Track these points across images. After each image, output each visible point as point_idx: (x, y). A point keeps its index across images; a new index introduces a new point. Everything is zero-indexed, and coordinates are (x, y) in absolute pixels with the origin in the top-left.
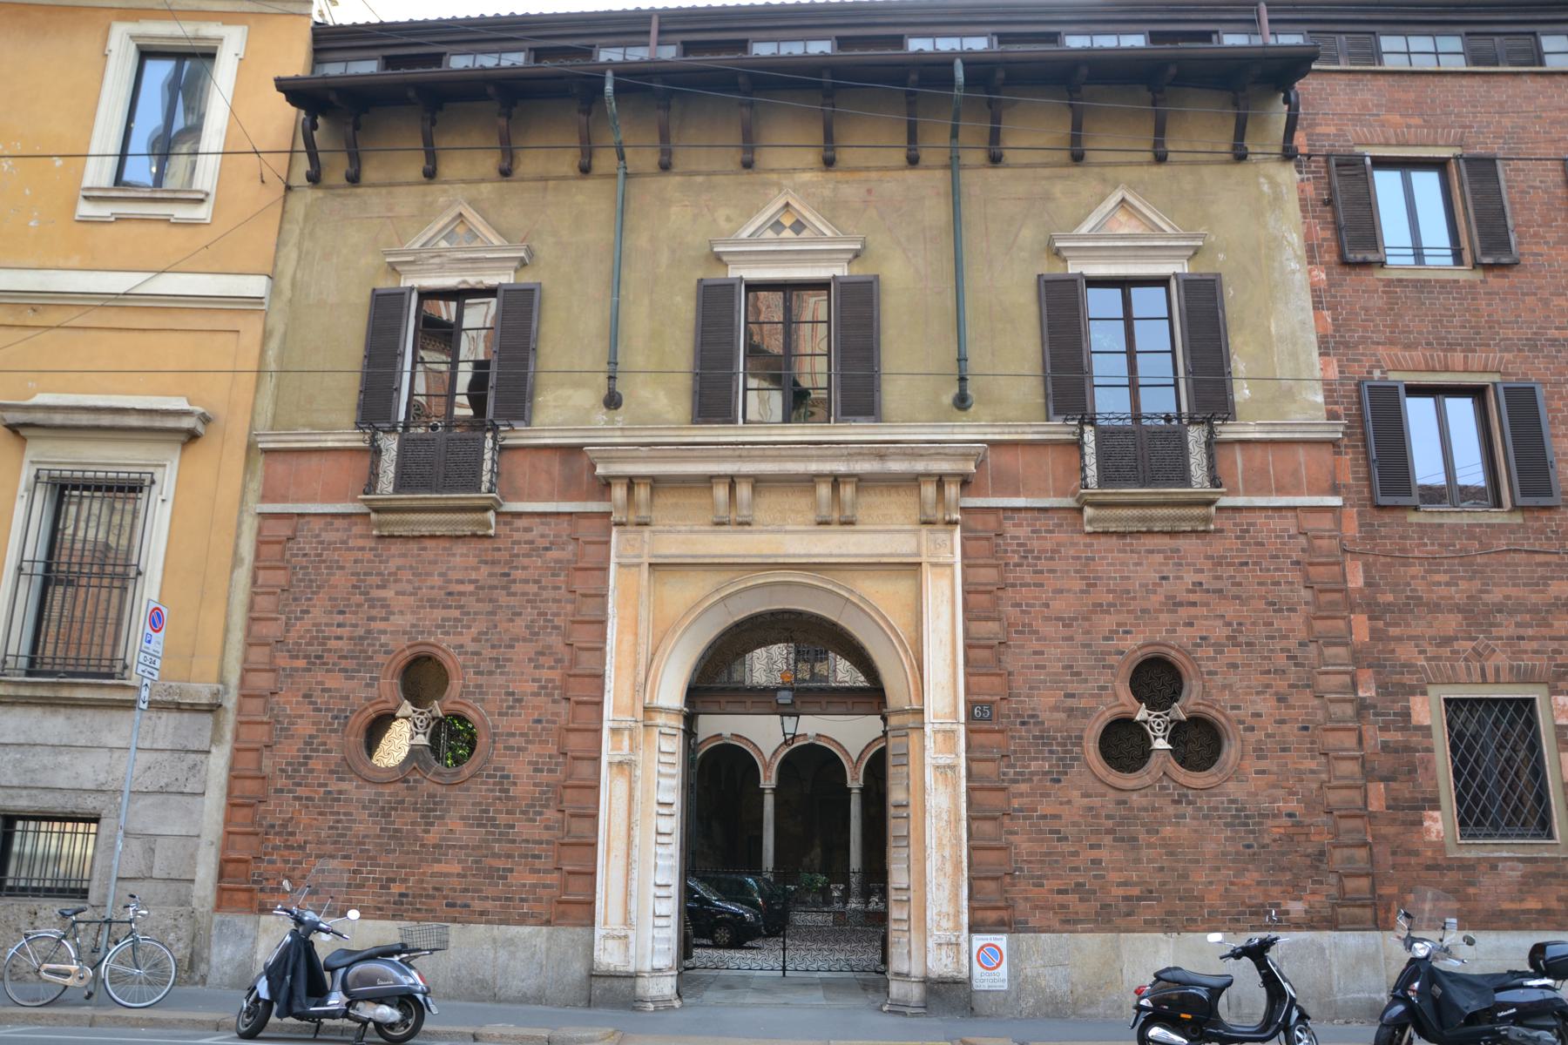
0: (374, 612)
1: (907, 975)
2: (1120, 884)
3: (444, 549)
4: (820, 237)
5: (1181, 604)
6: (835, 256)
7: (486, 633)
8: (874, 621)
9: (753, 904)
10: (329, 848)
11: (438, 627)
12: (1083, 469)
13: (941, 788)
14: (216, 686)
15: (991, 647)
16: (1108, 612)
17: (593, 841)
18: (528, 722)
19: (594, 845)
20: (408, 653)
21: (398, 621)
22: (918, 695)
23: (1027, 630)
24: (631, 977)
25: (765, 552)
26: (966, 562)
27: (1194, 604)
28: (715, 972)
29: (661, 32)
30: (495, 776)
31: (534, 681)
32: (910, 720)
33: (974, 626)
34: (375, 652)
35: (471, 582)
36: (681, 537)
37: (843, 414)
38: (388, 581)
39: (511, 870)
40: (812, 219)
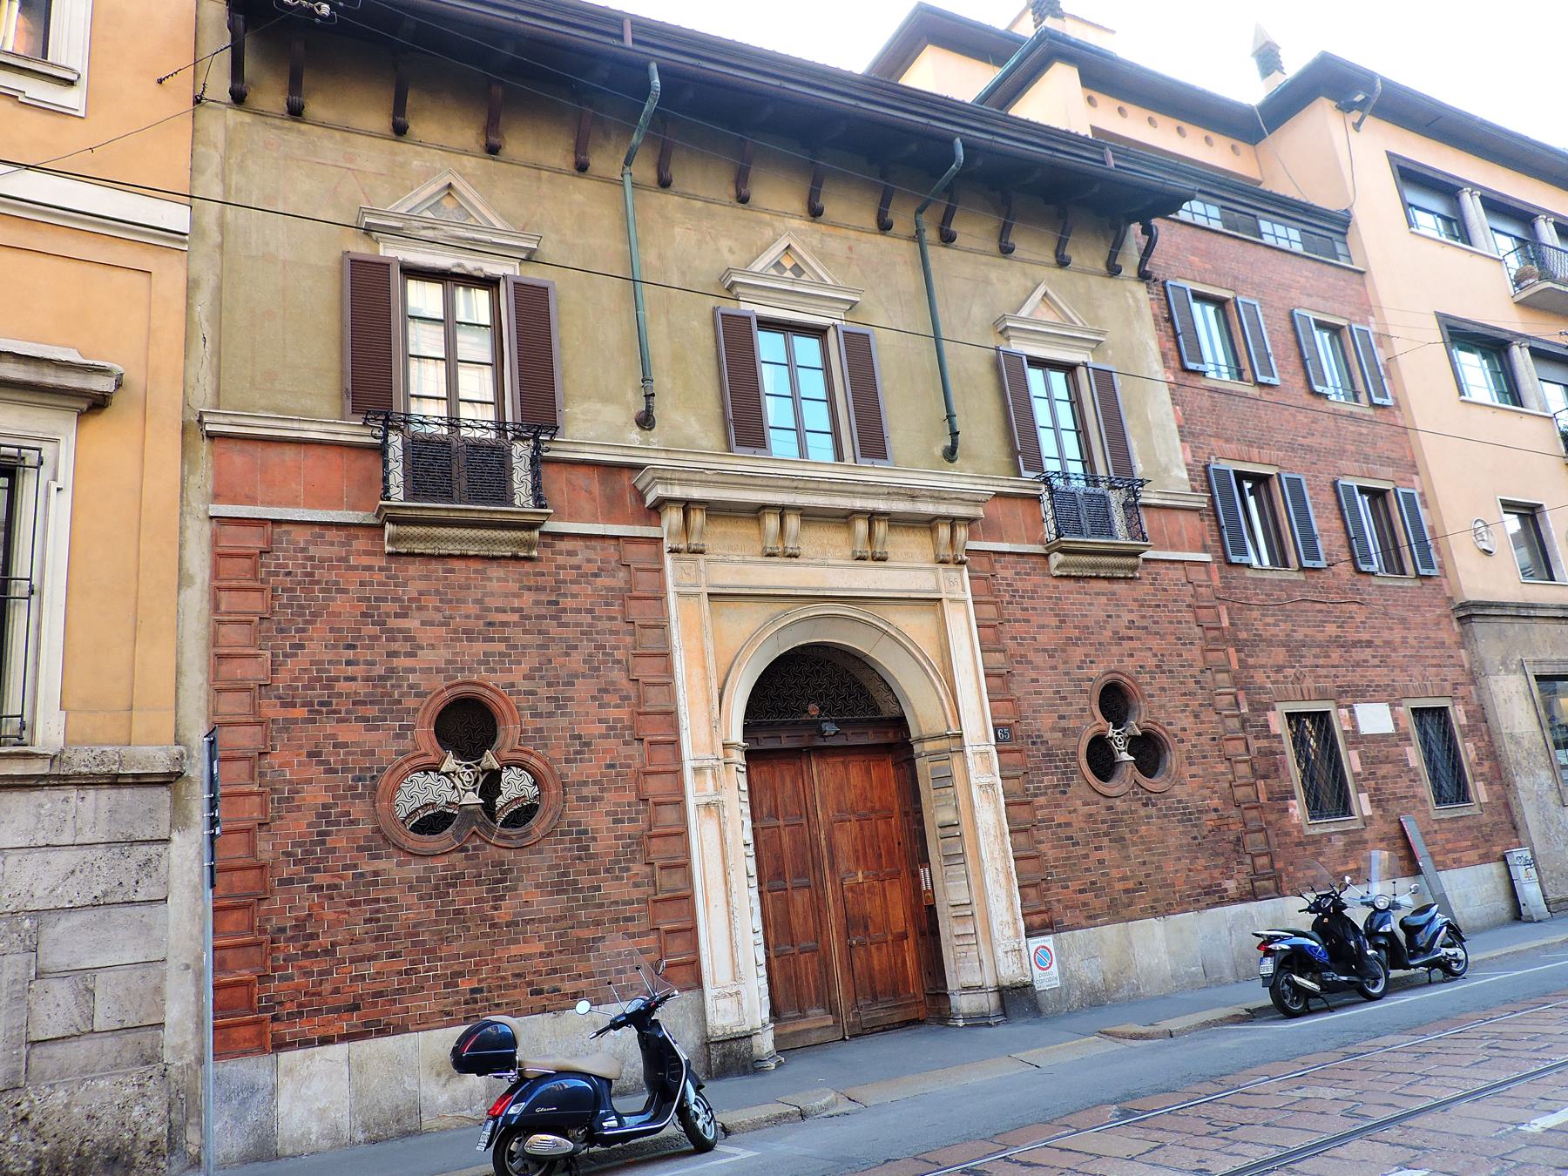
0: (395, 646)
2: (1121, 879)
3: (476, 571)
5: (1122, 638)
7: (540, 669)
10: (368, 947)
11: (480, 663)
13: (986, 805)
14: (176, 750)
17: (688, 892)
18: (600, 768)
20: (446, 694)
21: (427, 657)
23: (1023, 660)
27: (1131, 638)
31: (600, 721)
34: (402, 695)
35: (514, 610)
38: (409, 608)
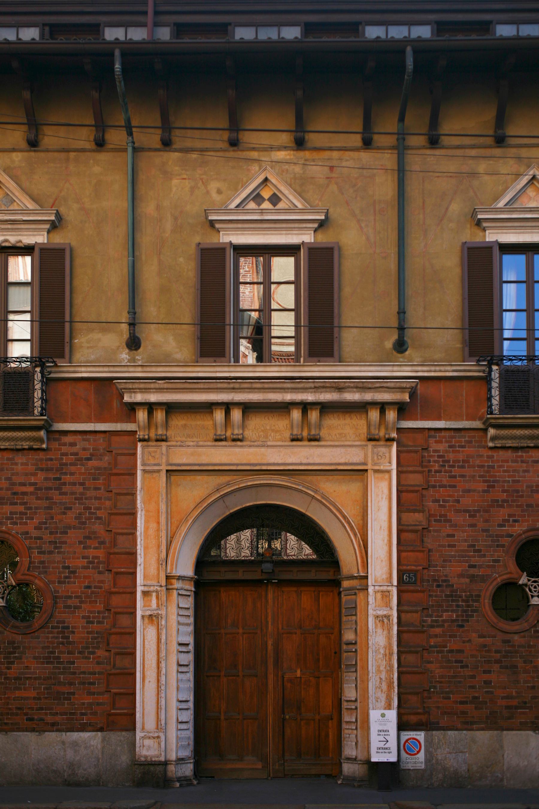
1: (355, 759)
2: (503, 698)
3: (8, 459)
4: (293, 209)
6: (304, 225)
7: (45, 523)
8: (332, 512)
11: (8, 518)
12: (489, 399)
13: (380, 631)
15: (416, 531)
16: (502, 506)
18: (81, 588)
22: (363, 566)
25: (252, 462)
29: (157, 13)
30: (58, 627)
31: (84, 558)
32: (354, 583)
35: (31, 484)
36: (190, 450)
39: (73, 694)
40: (286, 192)
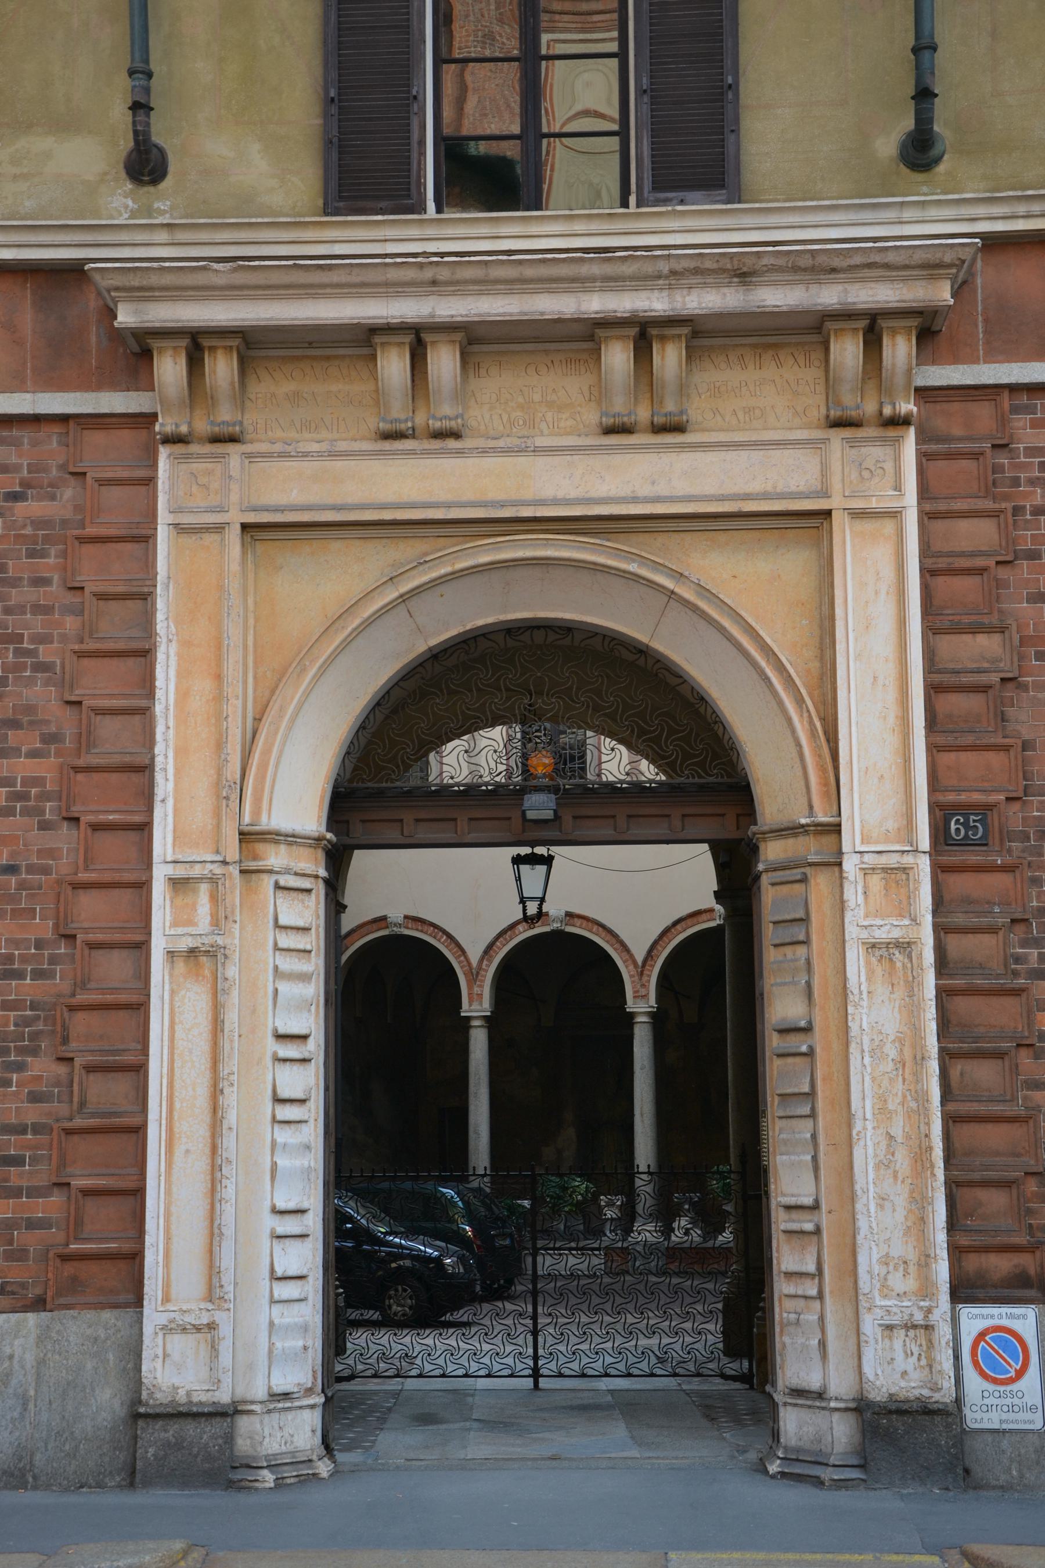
1: (820, 1395)
9: (456, 1238)
13: (882, 990)
15: (984, 689)
17: (135, 1121)
19: (139, 1131)
22: (826, 794)
24: (223, 1415)
25: (492, 495)
26: (928, 507)
28: (394, 1385)
32: (810, 848)
33: (946, 644)
36: (308, 467)
37: (657, 187)
